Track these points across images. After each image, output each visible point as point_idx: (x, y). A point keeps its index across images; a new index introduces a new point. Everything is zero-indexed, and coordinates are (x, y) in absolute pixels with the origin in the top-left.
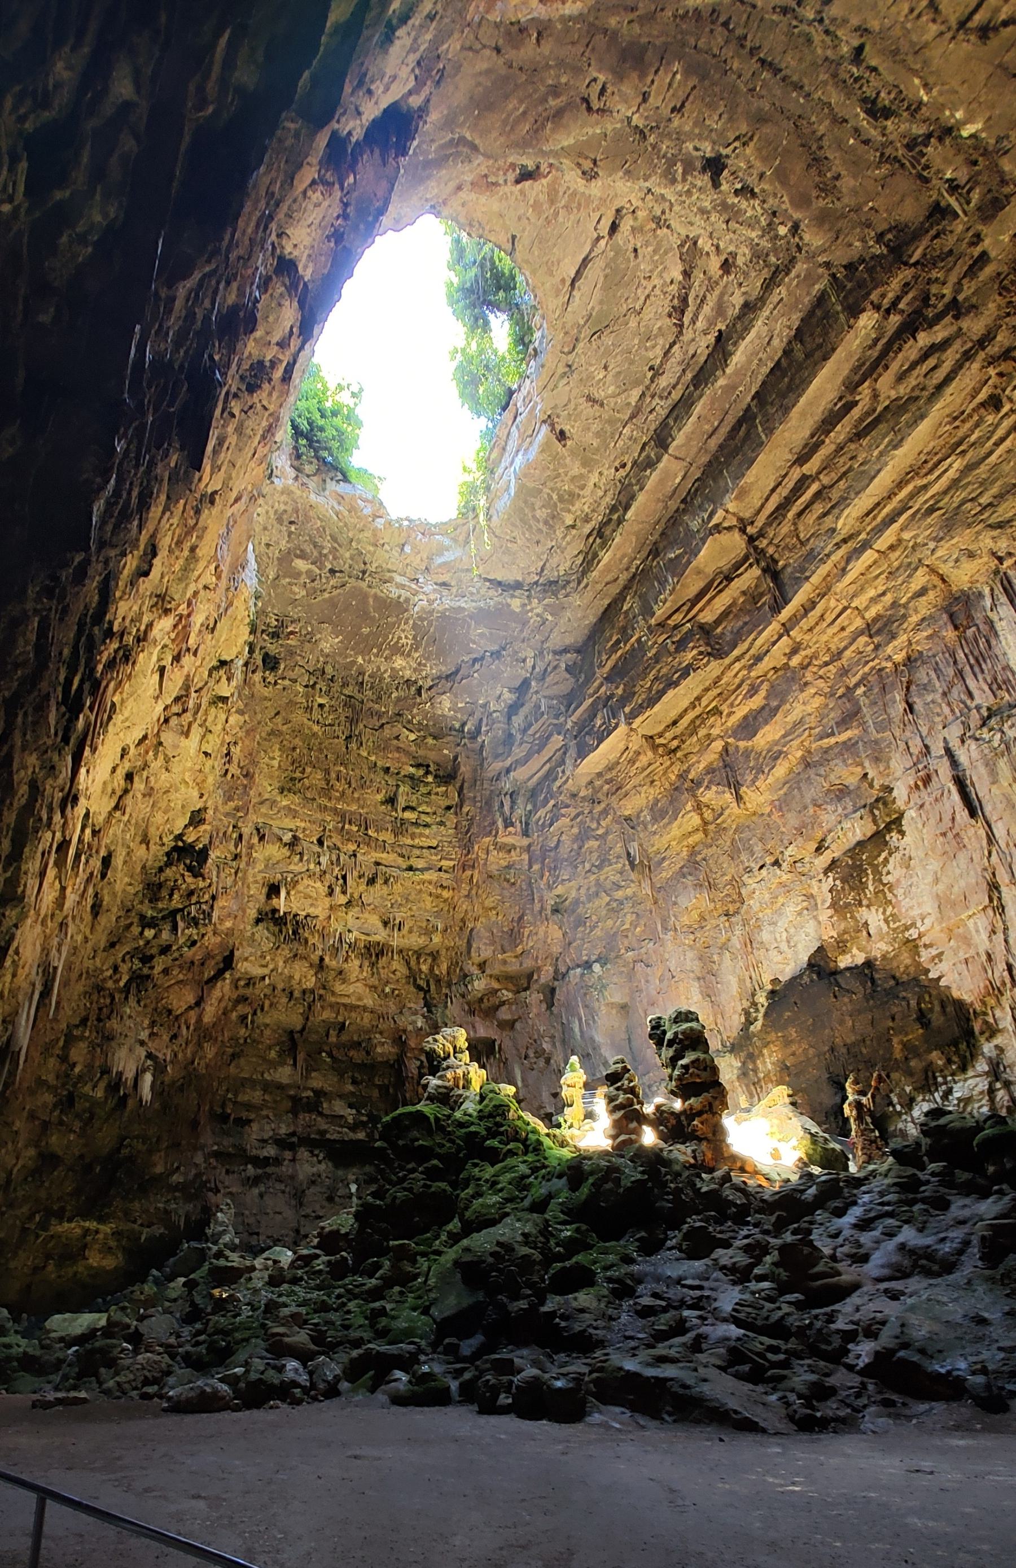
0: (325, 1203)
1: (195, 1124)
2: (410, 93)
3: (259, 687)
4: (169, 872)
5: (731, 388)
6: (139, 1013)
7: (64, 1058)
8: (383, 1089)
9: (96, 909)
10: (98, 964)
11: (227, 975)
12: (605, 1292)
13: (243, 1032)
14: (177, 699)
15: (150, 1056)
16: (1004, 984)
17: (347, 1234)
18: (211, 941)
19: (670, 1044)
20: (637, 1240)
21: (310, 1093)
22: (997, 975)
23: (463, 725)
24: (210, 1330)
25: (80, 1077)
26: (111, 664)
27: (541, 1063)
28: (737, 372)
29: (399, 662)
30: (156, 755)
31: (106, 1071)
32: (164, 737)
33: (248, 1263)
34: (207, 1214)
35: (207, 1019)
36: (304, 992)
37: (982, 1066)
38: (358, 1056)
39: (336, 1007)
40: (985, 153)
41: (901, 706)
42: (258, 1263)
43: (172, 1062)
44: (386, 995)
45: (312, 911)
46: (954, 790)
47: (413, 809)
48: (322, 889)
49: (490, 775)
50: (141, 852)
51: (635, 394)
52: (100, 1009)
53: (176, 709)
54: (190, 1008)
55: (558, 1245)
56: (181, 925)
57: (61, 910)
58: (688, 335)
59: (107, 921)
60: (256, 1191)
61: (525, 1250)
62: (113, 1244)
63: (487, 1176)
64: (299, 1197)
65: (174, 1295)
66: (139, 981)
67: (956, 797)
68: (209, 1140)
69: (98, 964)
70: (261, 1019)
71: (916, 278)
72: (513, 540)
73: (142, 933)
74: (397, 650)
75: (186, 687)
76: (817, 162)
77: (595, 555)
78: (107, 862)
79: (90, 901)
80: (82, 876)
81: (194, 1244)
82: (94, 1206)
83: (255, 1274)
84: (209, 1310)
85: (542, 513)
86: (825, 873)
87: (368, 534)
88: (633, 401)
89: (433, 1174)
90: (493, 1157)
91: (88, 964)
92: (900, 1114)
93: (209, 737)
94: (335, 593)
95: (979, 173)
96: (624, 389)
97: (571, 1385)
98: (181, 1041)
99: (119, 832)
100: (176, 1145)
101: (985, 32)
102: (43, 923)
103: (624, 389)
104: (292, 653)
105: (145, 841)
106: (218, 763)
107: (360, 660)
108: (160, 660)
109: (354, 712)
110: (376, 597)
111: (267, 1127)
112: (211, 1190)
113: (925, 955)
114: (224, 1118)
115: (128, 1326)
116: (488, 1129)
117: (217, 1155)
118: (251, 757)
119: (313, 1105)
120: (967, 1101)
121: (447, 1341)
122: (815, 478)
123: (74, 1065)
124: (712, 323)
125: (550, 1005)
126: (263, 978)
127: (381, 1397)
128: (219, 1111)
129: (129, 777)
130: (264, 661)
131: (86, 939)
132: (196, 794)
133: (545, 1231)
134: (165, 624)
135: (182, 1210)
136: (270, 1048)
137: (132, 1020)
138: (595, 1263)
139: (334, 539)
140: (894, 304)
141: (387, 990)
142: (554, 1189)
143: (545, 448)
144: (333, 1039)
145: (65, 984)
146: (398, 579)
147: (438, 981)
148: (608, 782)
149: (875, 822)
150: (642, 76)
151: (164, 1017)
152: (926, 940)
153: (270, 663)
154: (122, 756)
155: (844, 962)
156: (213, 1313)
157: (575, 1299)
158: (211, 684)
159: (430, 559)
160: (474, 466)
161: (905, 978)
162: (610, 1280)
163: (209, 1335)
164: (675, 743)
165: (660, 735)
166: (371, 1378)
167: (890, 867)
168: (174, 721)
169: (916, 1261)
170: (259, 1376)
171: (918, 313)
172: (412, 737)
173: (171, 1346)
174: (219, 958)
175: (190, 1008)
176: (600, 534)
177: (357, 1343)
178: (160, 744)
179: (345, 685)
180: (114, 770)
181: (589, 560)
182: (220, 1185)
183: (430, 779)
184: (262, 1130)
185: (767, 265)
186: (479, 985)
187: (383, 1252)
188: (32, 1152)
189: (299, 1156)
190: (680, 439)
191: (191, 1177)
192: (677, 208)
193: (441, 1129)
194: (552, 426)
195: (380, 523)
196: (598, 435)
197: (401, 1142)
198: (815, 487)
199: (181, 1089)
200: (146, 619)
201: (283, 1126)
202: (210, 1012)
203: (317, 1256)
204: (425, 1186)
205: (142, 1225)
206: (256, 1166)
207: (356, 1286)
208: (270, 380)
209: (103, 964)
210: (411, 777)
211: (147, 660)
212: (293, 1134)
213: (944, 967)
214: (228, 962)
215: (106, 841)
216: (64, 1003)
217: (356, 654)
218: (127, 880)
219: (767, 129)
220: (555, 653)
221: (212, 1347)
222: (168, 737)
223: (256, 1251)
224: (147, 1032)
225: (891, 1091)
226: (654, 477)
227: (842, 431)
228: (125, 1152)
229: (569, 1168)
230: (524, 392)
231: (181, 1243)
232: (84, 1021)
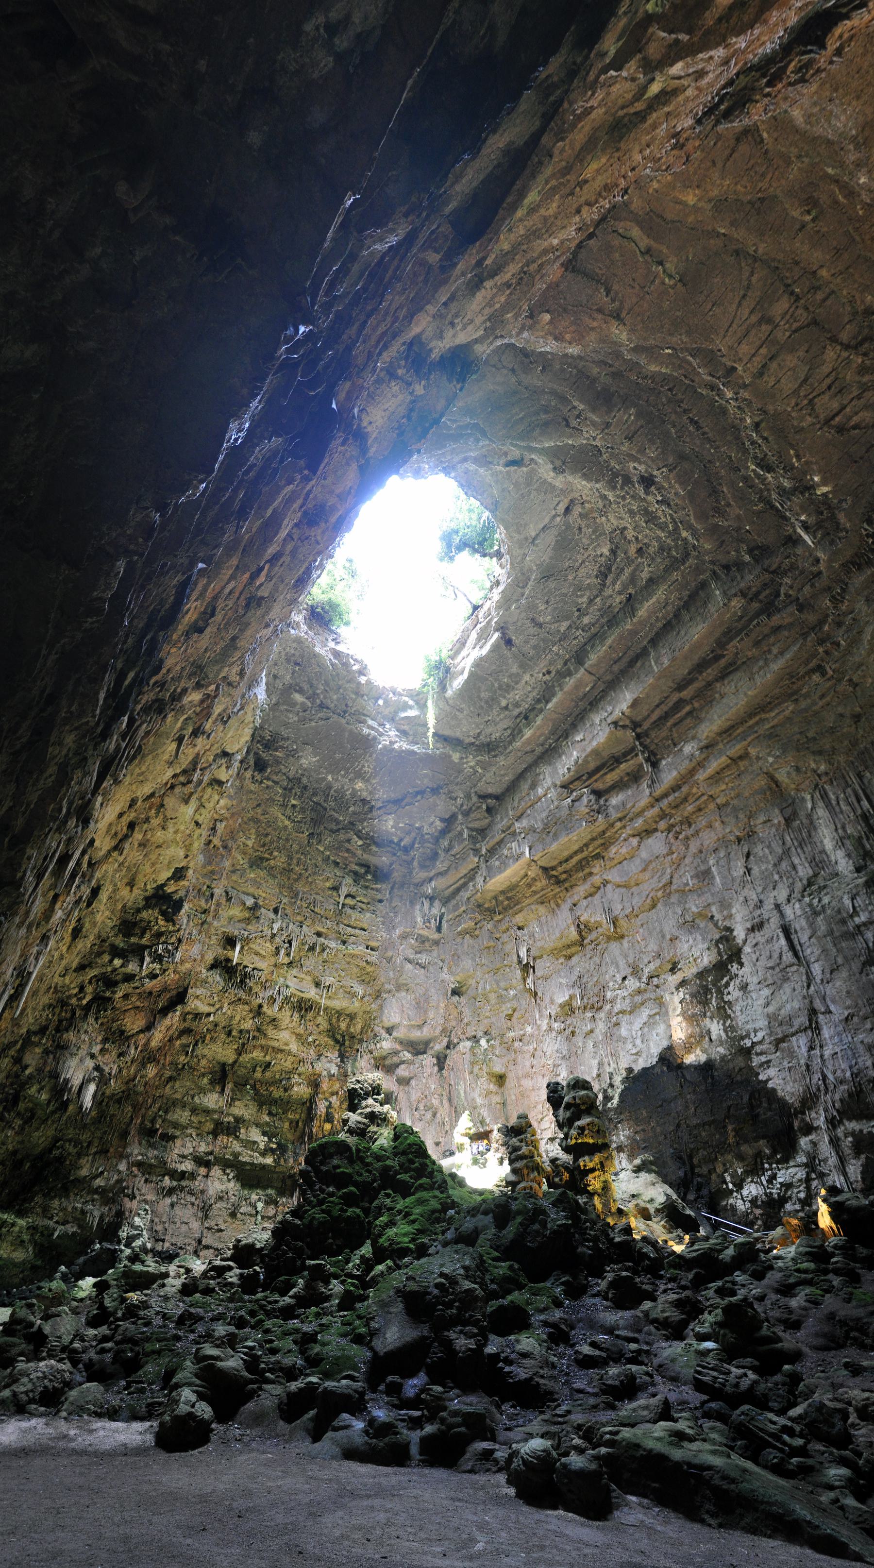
0: (229, 1219)
1: (124, 1135)
2: (476, 341)
3: (248, 782)
4: (145, 914)
5: (633, 633)
6: (94, 1030)
7: (17, 1060)
8: (294, 1124)
9: (76, 933)
10: (67, 981)
11: (179, 1008)
12: (545, 1337)
13: (182, 1059)
14: (184, 772)
15: (97, 1068)
16: (819, 1089)
17: (262, 1249)
18: (171, 977)
19: (568, 1106)
20: (562, 1284)
21: (231, 1119)
22: (814, 1081)
23: (401, 840)
24: (118, 1338)
25: (31, 1077)
26: (146, 710)
27: (429, 1115)
28: (640, 623)
29: (359, 785)
30: (157, 813)
31: (55, 1075)
32: (167, 800)
33: (163, 1269)
34: (120, 1217)
35: (153, 1044)
36: (241, 1031)
37: (801, 1159)
38: (277, 1093)
39: (265, 1049)
40: (830, 508)
41: (742, 871)
42: (172, 1269)
43: (116, 1076)
44: (309, 1044)
46: (781, 935)
47: (353, 897)
48: (269, 947)
49: (416, 881)
50: (125, 892)
51: (565, 625)
52: (60, 1021)
53: (182, 779)
54: (142, 1031)
55: (492, 1281)
56: (147, 959)
57: (47, 922)
58: (608, 592)
59: (84, 945)
60: (168, 1201)
61: (467, 1285)
62: (26, 1237)
63: (399, 1207)
64: (205, 1210)
65: (81, 1295)
66: (101, 1002)
67: (783, 941)
68: (136, 1151)
69: (67, 981)
70: (201, 1050)
71: (772, 581)
72: (461, 710)
73: (111, 961)
74: (360, 775)
75: (195, 763)
76: (714, 492)
77: (520, 731)
78: (95, 892)
79: (73, 924)
80: (71, 899)
81: (107, 1245)
83: (169, 1281)
84: (120, 1314)
85: (485, 695)
86: (677, 989)
87: (353, 685)
88: (562, 630)
89: (349, 1200)
90: (405, 1190)
91: (57, 979)
92: (731, 1192)
93: (202, 810)
94: (321, 723)
95: (823, 521)
96: (558, 620)
97: (593, 1466)
98: (128, 1058)
99: (111, 870)
100: (104, 1152)
101: (841, 430)
102: (30, 927)
103: (558, 620)
104: (278, 762)
106: (204, 832)
107: (330, 778)
108: (182, 729)
110: (351, 732)
111: (189, 1145)
112: (128, 1196)
113: (756, 1061)
114: (152, 1132)
115: (32, 1325)
116: (401, 1165)
117: (139, 1164)
118: (232, 834)
119: (231, 1129)
120: (788, 1186)
121: (390, 1378)
122: (690, 702)
123: (26, 1067)
124: (625, 587)
125: (441, 1068)
126: (209, 1015)
127: (329, 1443)
128: (149, 1125)
129: (132, 826)
130: (256, 764)
131: (62, 957)
132: (182, 853)
133: (481, 1265)
134: (195, 697)
135: (96, 1213)
136: (203, 1075)
138: (528, 1304)
139: (327, 683)
140: (758, 594)
141: (310, 1039)
142: (480, 1224)
143: (495, 648)
144: (258, 1074)
145: (34, 993)
146: (370, 722)
147: (353, 1037)
148: (508, 899)
149: (719, 954)
150: (609, 412)
151: (117, 1037)
152: (758, 1049)
153: (260, 766)
154: (130, 806)
155: (690, 1059)
156: (124, 1318)
157: (518, 1341)
158: (214, 767)
159: (396, 712)
160: (330, 595)
161: (739, 1078)
162: (546, 1324)
163: (117, 1343)
164: (564, 876)
165: (553, 868)
166: (311, 1419)
167: (731, 989)
168: (177, 790)
169: (847, 1333)
170: (188, 1409)
171: (771, 604)
172: (360, 843)
173: (75, 1351)
174: (174, 993)
175: (142, 1031)
176: (526, 718)
177: (291, 1374)
178: (162, 805)
179: (315, 794)
180: (121, 815)
181: (515, 732)
182: (136, 1192)
183: (369, 877)
184: (184, 1146)
185: (670, 556)
186: (386, 1045)
187: (297, 1272)
189: (212, 1173)
190: (593, 658)
191: (112, 1182)
192: (614, 506)
193: (362, 1159)
194: (503, 634)
195: (363, 680)
196: (534, 647)
197: (324, 1168)
198: (688, 708)
199: (119, 1101)
200: (183, 684)
201: (203, 1144)
202: (158, 1037)
203: (230, 1268)
204: (342, 1210)
205: (57, 1222)
206: (172, 1178)
207: (270, 1303)
208: (326, 522)
209: (71, 982)
210: (356, 873)
211: (173, 723)
212: (211, 1153)
213: (772, 1072)
214: (180, 997)
215: (98, 874)
216: (29, 1011)
217: (328, 773)
218: (107, 913)
219: (686, 465)
220: (480, 797)
221: (118, 1355)
222: (170, 802)
223: (168, 1257)
224: (99, 1047)
225: (726, 1171)
226: (570, 683)
227: (710, 673)
228: (56, 1153)
229: (498, 1206)
230: (486, 608)
231: (93, 1243)
232: (43, 1030)
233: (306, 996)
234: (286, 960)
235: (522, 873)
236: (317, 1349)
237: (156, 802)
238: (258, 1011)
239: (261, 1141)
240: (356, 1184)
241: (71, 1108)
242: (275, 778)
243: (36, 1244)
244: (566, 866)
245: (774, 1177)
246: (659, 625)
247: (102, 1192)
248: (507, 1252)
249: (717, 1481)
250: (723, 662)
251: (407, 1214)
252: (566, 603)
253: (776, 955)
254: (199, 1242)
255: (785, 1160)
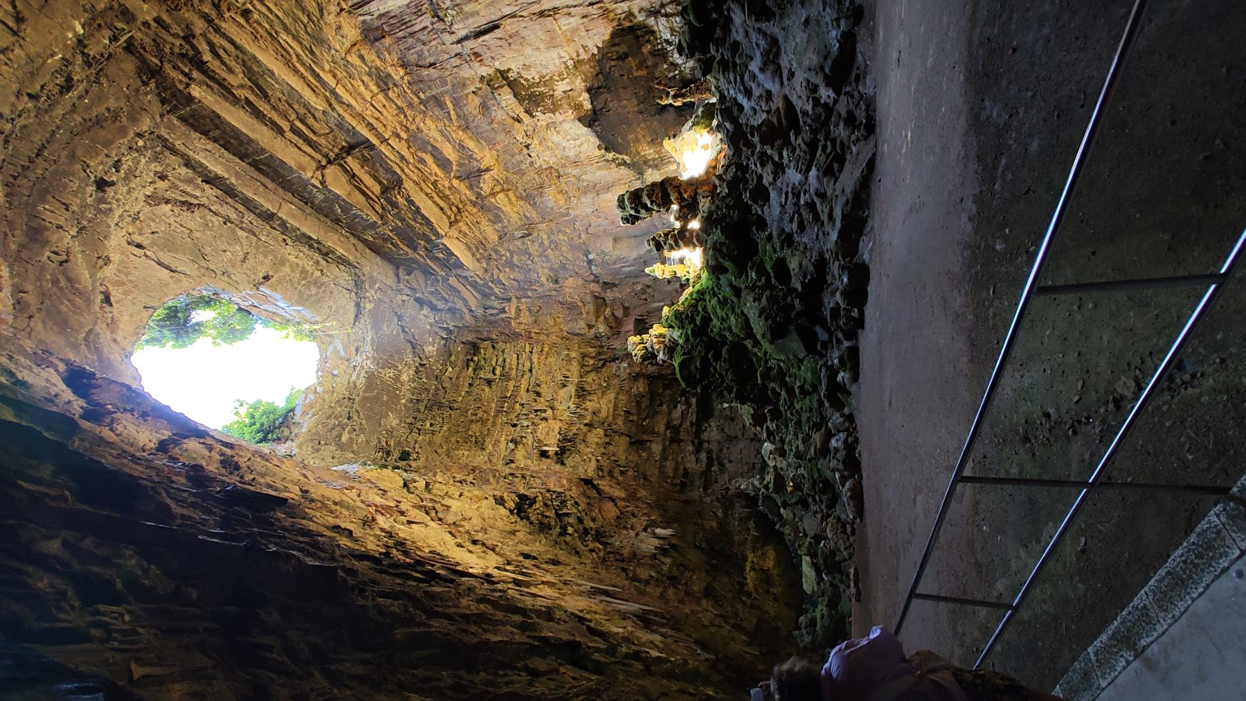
1: (687, 502)
2: (57, 371)
4: (533, 518)
5: (237, 175)
7: (647, 582)
8: (665, 387)
9: (555, 562)
14: (427, 513)
15: (645, 530)
18: (575, 492)
26: (406, 553)
27: (649, 290)
28: (228, 171)
29: (405, 377)
31: (654, 557)
34: (742, 495)
35: (623, 495)
37: (651, 21)
38: (645, 403)
39: (615, 416)
40: (94, 19)
42: (771, 464)
45: (556, 431)
46: (482, 38)
50: (520, 535)
51: (240, 233)
53: (433, 514)
56: (565, 511)
58: (204, 201)
59: (562, 556)
60: (728, 465)
61: (764, 300)
62: (760, 553)
64: (731, 439)
66: (599, 536)
67: (487, 37)
68: (696, 494)
70: (622, 462)
71: (170, 62)
74: (397, 379)
76: (99, 122)
78: (526, 556)
79: (551, 566)
82: (737, 564)
85: (314, 290)
87: (326, 397)
89: (717, 357)
90: (707, 320)
91: (589, 567)
96: (237, 240)
98: (636, 511)
101: (19, 19)
103: (237, 240)
105: (514, 532)
106: (466, 488)
109: (435, 405)
110: (365, 392)
113: (584, 56)
114: (683, 484)
117: (705, 489)
120: (672, 30)
122: (292, 123)
124: (197, 186)
125: (614, 285)
127: (853, 388)
129: (475, 542)
131: (574, 569)
133: (752, 288)
134: (382, 521)
135: (739, 510)
137: (623, 540)
139: (329, 417)
140: (186, 75)
143: (273, 288)
144: (635, 418)
145: (601, 581)
146: (354, 378)
147: (599, 354)
149: (502, 87)
150: (47, 229)
151: (621, 521)
153: (405, 456)
155: (588, 105)
160: (285, 332)
162: (782, 249)
167: (530, 77)
168: (441, 515)
171: (191, 60)
176: (326, 254)
177: (821, 403)
180: (470, 552)
181: (342, 261)
185: (161, 153)
186: (602, 328)
188: (704, 602)
192: (127, 208)
196: (265, 256)
198: (298, 123)
199: (665, 511)
202: (618, 493)
209: (589, 558)
210: (475, 370)
211: (403, 531)
212: (693, 442)
214: (588, 482)
219: (79, 152)
223: (764, 465)
226: (292, 222)
227: (263, 107)
228: (704, 545)
232: (624, 570)
233: (573, 391)
234: (550, 412)
235: (456, 241)
236: (807, 387)
237: (454, 529)
238: (590, 425)
239: (681, 408)
240: (706, 354)
241: (674, 541)
242: (412, 444)
243: (214, 479)
244: (446, 207)
245: (667, 41)
246: (226, 154)
247: (726, 510)
248: (741, 271)
249: (848, 208)
250: (252, 98)
251: (723, 319)
252: (221, 235)
253: (500, 43)
254: (752, 440)
255: (653, 32)
